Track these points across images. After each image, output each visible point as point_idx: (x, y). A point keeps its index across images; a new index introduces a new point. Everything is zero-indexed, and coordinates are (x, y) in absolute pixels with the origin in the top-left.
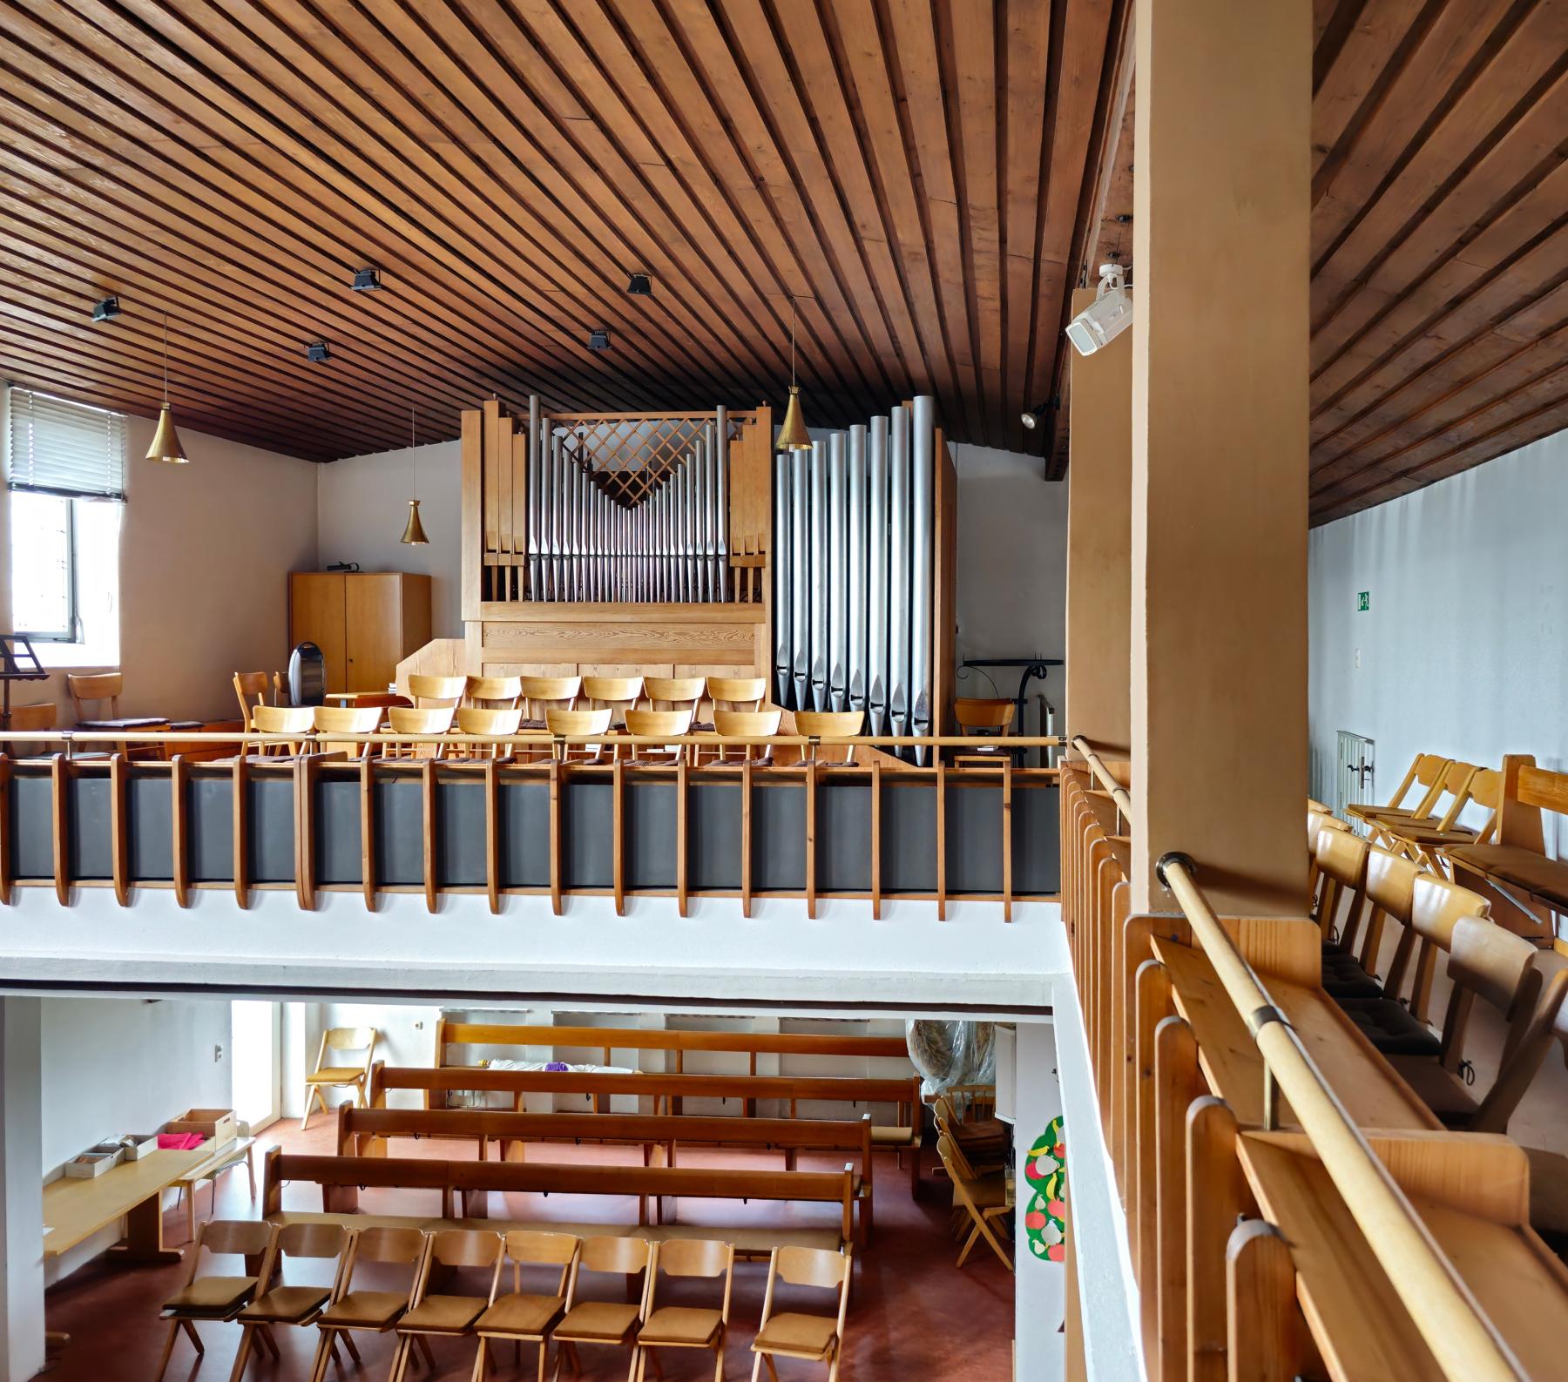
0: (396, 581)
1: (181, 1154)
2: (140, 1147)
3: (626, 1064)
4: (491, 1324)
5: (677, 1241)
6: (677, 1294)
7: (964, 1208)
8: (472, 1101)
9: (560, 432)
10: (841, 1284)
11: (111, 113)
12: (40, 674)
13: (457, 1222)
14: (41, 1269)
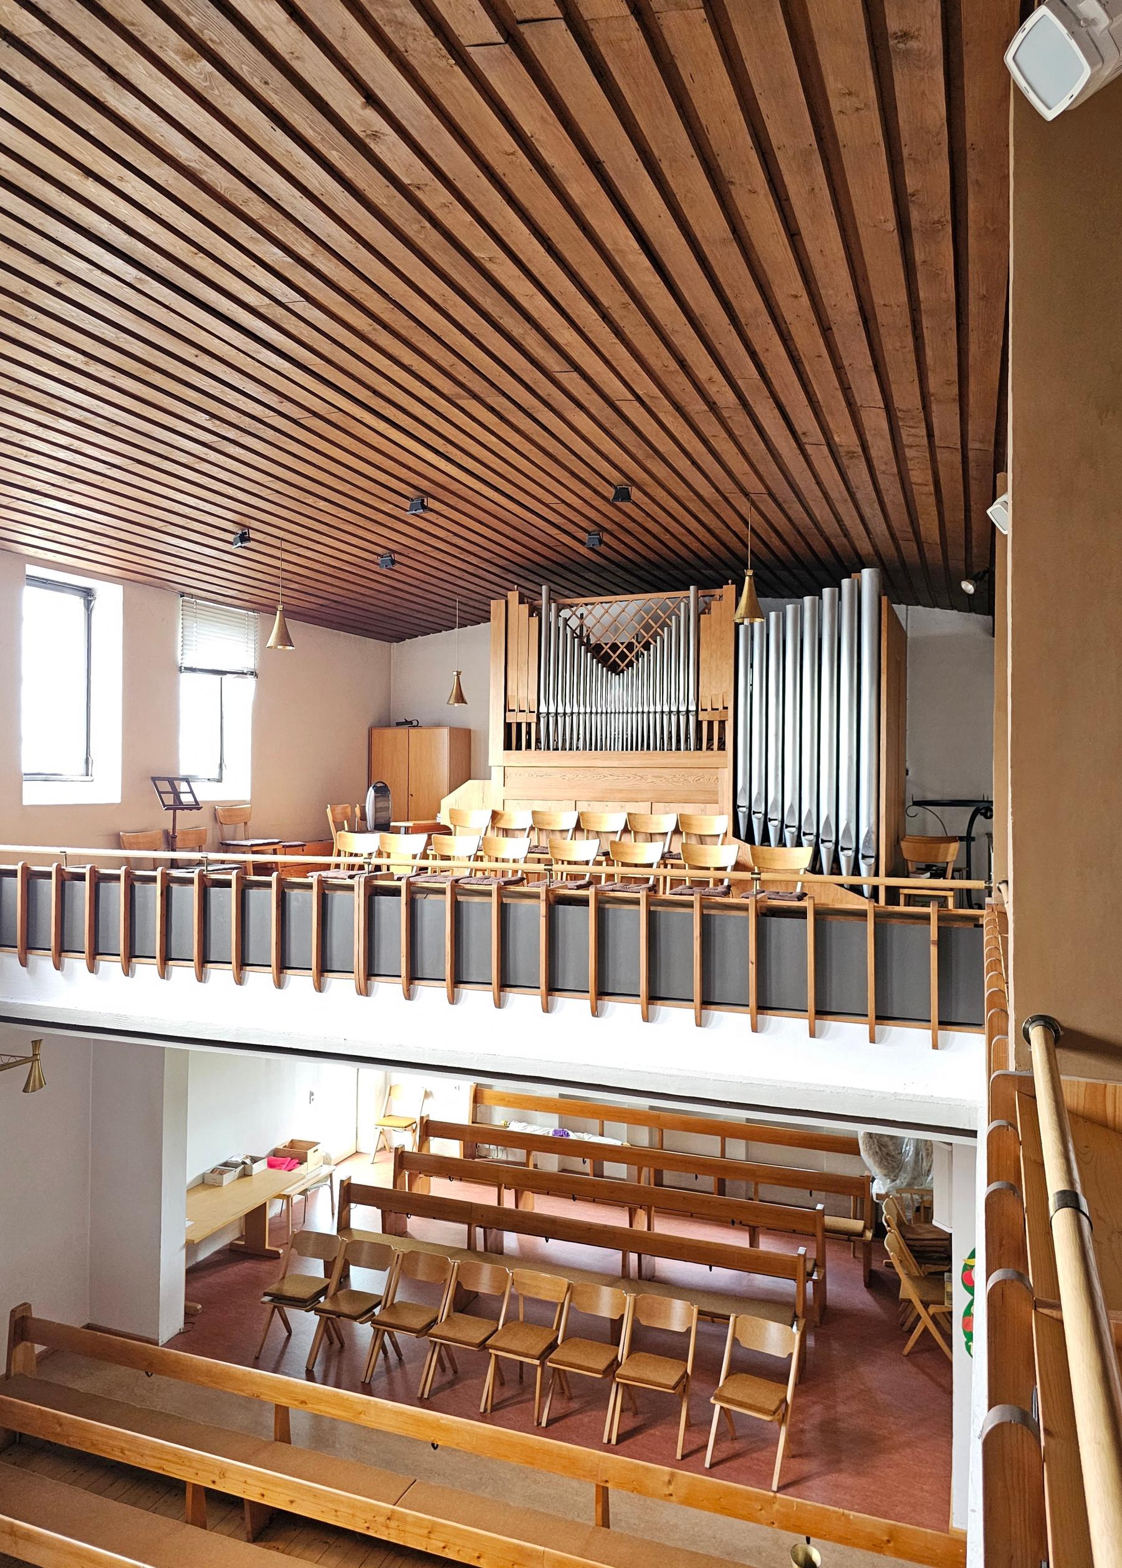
0: (445, 732)
1: (281, 1174)
2: (254, 1166)
3: (616, 1136)
4: (499, 1344)
5: (653, 1297)
6: (647, 1341)
7: (910, 1301)
8: (497, 1154)
9: (565, 613)
10: (791, 1355)
11: (238, 400)
12: (196, 806)
13: (479, 1254)
14: (184, 1251)
